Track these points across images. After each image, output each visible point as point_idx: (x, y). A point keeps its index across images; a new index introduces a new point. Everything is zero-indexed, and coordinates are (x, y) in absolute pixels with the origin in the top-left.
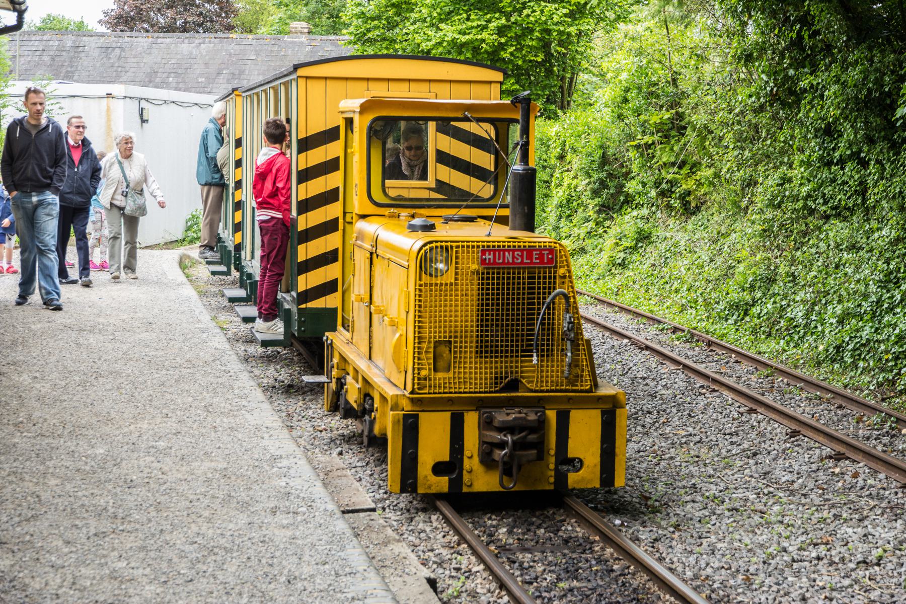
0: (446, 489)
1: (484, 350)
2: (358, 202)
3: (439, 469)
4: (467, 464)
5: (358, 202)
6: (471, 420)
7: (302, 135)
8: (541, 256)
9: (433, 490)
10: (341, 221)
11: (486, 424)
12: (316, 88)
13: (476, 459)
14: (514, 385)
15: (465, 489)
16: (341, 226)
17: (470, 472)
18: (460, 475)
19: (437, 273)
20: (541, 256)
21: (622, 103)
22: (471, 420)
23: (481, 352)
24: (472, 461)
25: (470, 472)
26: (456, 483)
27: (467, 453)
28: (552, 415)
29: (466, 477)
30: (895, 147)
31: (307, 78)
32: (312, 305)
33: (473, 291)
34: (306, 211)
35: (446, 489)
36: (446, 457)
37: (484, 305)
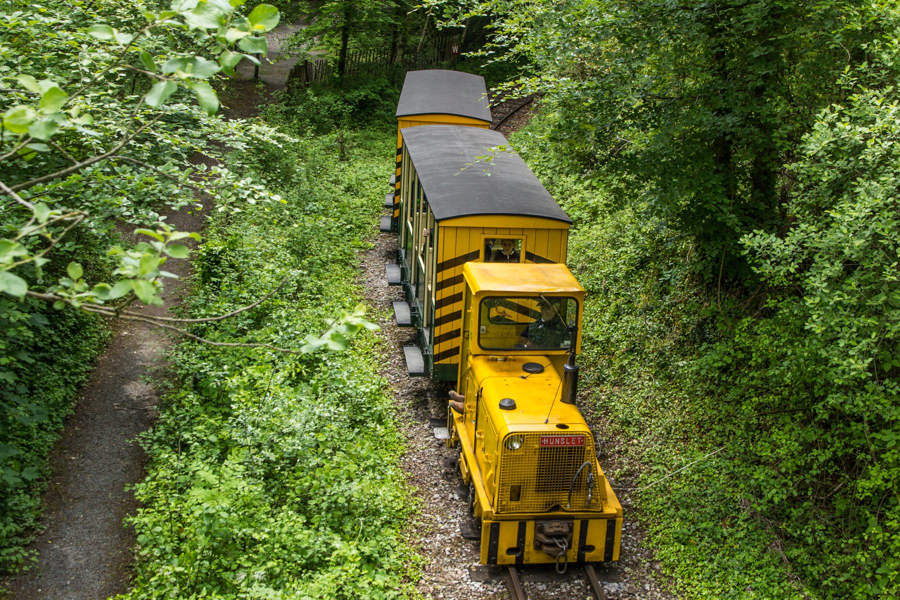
0: (514, 562)
1: (541, 488)
2: (473, 346)
3: (510, 551)
4: (526, 550)
5: (473, 346)
6: (530, 527)
7: (440, 261)
8: (576, 441)
9: (506, 563)
10: (462, 331)
11: (539, 530)
12: (450, 234)
13: (532, 547)
14: (557, 508)
15: (524, 562)
16: (464, 297)
17: (528, 553)
18: (522, 555)
19: (513, 449)
20: (576, 441)
21: (636, 244)
22: (530, 527)
23: (537, 491)
24: (529, 547)
25: (528, 553)
26: (519, 559)
27: (527, 543)
28: (577, 524)
29: (525, 556)
30: (797, 16)
31: (444, 227)
32: (441, 362)
33: (535, 459)
34: (440, 342)
35: (514, 562)
36: (515, 545)
37: (540, 466)
